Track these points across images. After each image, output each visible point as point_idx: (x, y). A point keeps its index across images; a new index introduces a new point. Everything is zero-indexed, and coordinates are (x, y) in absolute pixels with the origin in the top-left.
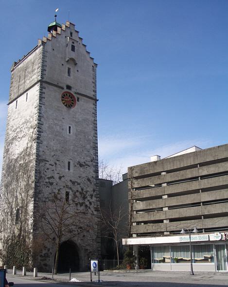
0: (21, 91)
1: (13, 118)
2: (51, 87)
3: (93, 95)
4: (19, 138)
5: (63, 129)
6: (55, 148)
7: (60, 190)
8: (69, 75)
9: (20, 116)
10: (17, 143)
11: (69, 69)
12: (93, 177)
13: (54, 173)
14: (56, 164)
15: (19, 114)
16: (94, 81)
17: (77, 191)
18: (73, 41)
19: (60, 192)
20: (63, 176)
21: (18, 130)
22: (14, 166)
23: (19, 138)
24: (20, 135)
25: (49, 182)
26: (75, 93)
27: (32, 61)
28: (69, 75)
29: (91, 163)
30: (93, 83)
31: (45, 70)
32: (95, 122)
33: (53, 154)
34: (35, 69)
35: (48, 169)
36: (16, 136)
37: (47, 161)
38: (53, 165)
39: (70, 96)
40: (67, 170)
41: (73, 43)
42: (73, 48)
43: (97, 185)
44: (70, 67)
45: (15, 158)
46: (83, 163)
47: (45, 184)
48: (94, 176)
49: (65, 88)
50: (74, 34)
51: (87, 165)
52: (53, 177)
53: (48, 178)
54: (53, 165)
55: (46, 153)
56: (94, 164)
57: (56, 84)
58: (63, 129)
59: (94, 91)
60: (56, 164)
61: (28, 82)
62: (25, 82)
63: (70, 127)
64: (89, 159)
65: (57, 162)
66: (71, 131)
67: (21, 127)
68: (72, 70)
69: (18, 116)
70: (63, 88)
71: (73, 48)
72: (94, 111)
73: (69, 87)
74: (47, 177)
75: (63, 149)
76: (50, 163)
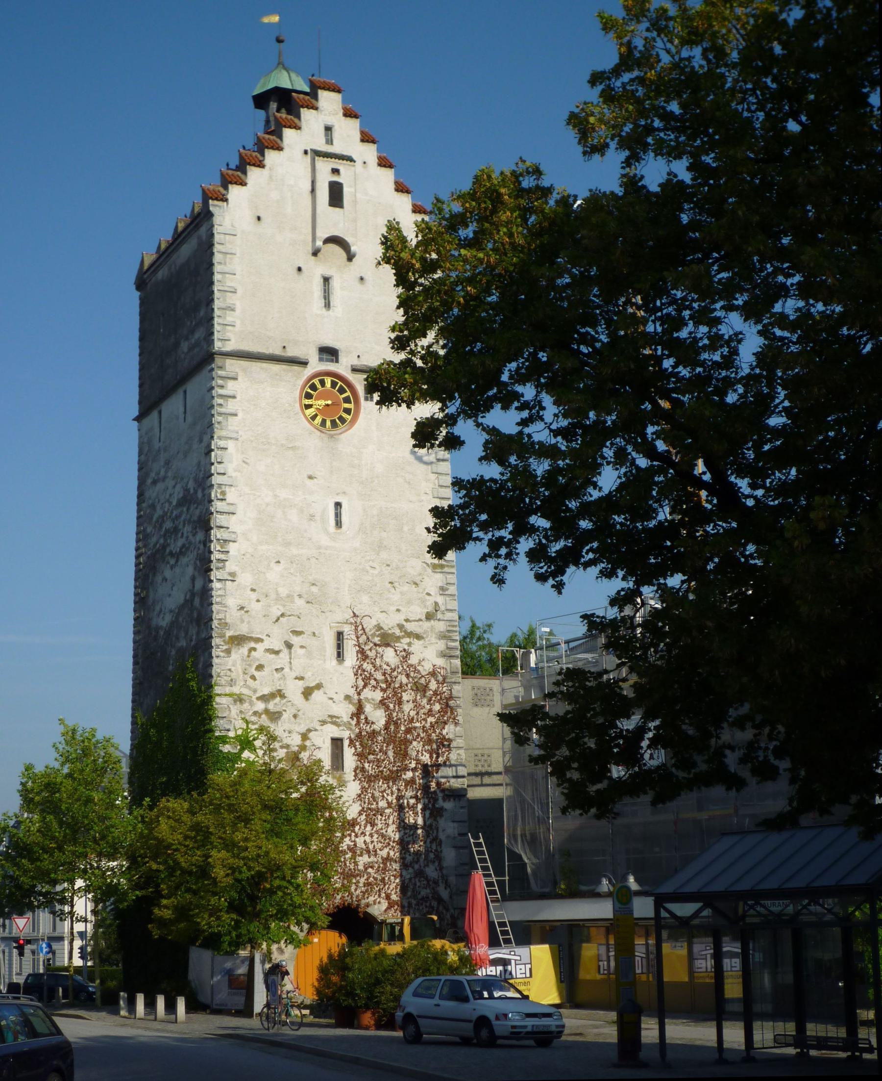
1: (153, 475)
2: (256, 366)
4: (171, 554)
5: (312, 517)
7: (311, 735)
8: (328, 305)
9: (170, 474)
10: (168, 573)
11: (326, 280)
14: (289, 646)
15: (167, 463)
19: (308, 743)
20: (319, 686)
24: (176, 545)
25: (267, 711)
26: (355, 370)
28: (328, 305)
29: (427, 625)
31: (233, 310)
33: (276, 611)
35: (260, 667)
36: (164, 547)
37: (259, 640)
38: (277, 653)
39: (334, 384)
40: (334, 662)
44: (327, 274)
46: (398, 632)
49: (313, 357)
51: (409, 634)
52: (280, 694)
54: (277, 653)
55: (253, 613)
57: (278, 351)
60: (289, 646)
61: (185, 346)
62: (177, 345)
63: (338, 505)
64: (418, 611)
65: (295, 640)
66: (344, 518)
67: (175, 513)
68: (335, 284)
69: (166, 472)
70: (304, 363)
73: (329, 353)
74: (259, 694)
75: (314, 589)
76: (267, 644)
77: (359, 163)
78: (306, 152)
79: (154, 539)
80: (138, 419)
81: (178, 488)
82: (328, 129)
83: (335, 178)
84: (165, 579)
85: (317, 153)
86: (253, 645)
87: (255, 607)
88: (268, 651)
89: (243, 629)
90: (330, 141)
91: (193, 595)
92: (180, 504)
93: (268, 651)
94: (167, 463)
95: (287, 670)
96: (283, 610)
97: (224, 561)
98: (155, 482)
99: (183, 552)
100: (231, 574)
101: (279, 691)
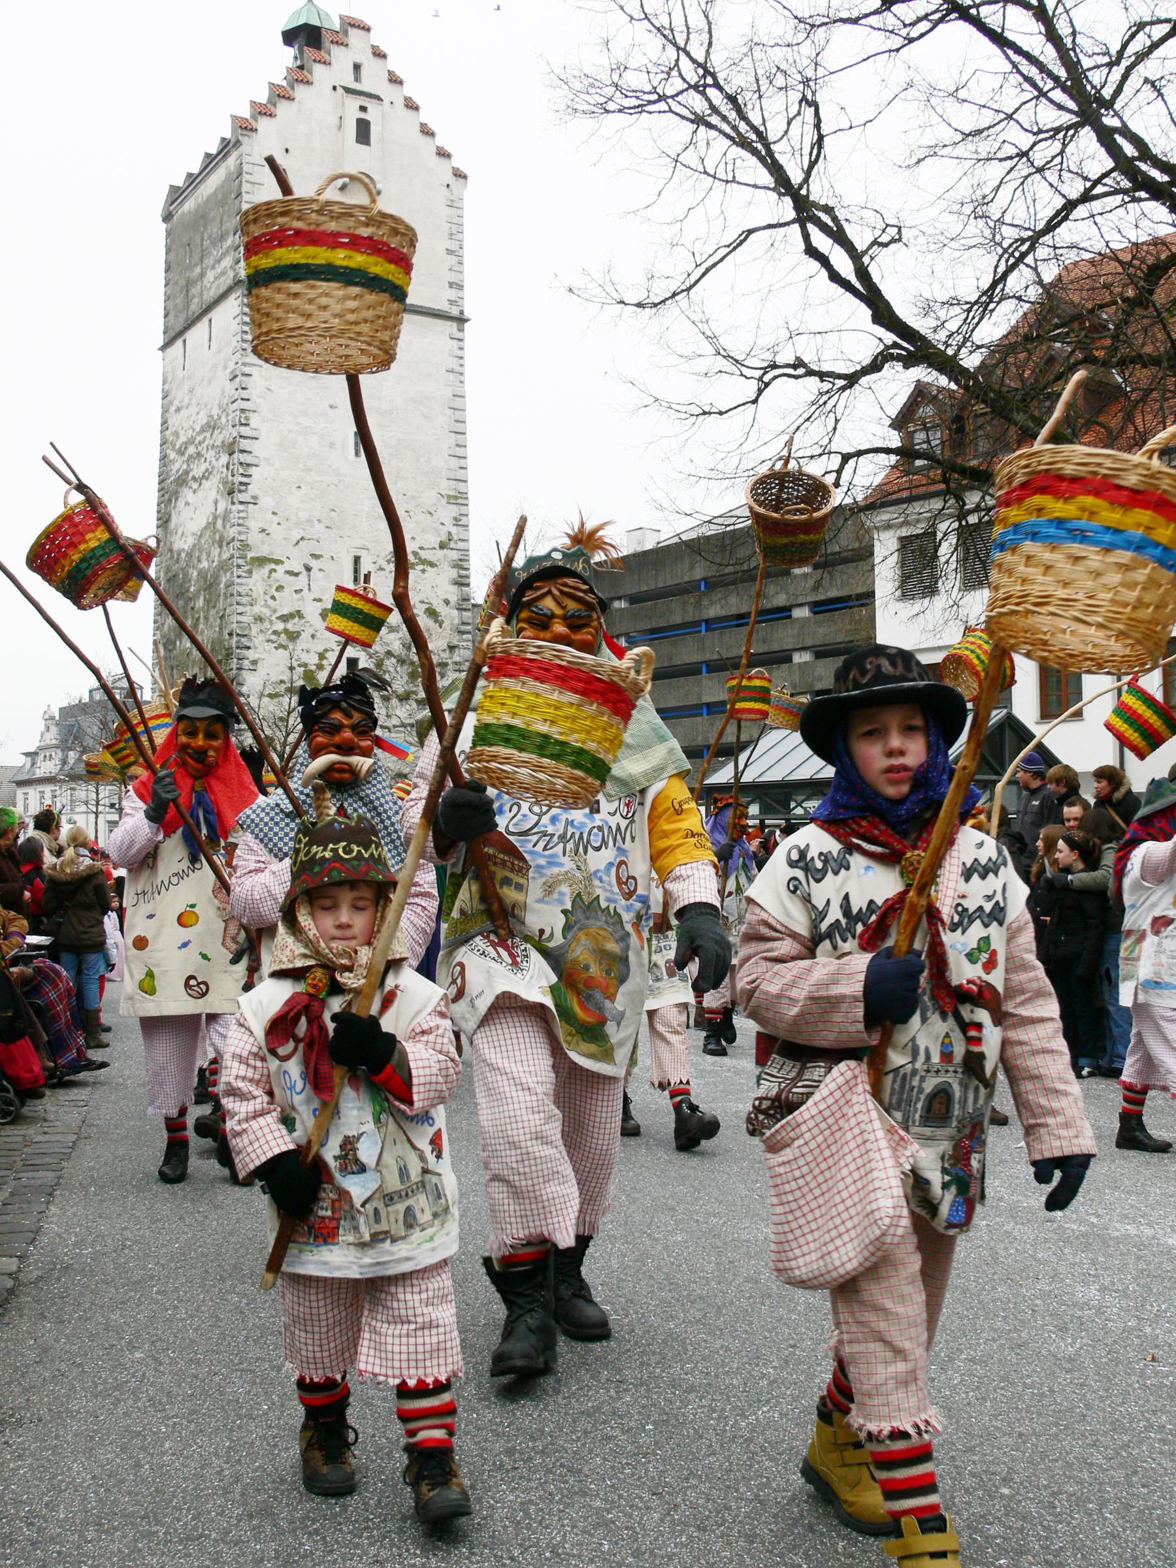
0: (195, 307)
3: (451, 302)
4: (194, 479)
6: (304, 516)
9: (194, 401)
12: (447, 602)
13: (302, 599)
14: (308, 569)
15: (191, 391)
16: (453, 246)
17: (389, 654)
18: (363, 101)
21: (191, 450)
22: (186, 575)
23: (194, 479)
24: (198, 470)
25: (286, 631)
27: (220, 196)
29: (440, 553)
30: (450, 252)
32: (457, 403)
34: (227, 233)
35: (280, 588)
38: (297, 575)
41: (363, 109)
42: (363, 132)
43: (463, 628)
45: (186, 547)
47: (273, 637)
48: (453, 599)
50: (370, 66)
52: (299, 614)
53: (284, 618)
54: (297, 575)
56: (454, 555)
58: (332, 446)
59: (451, 285)
60: (308, 569)
61: (210, 275)
62: (202, 275)
65: (314, 564)
67: (199, 438)
71: (363, 132)
72: (453, 364)
74: (279, 614)
75: (333, 514)
76: (287, 566)
77: (386, 103)
78: (335, 88)
79: (177, 466)
80: (163, 348)
81: (202, 414)
82: (357, 67)
83: (363, 115)
84: (187, 504)
85: (348, 90)
86: (273, 566)
87: (273, 528)
88: (287, 572)
89: (264, 551)
90: (357, 79)
91: (215, 518)
92: (203, 430)
93: (287, 572)
94: (191, 391)
95: (306, 591)
96: (302, 534)
97: (246, 484)
98: (178, 410)
99: (206, 476)
100: (254, 497)
101: (298, 612)
